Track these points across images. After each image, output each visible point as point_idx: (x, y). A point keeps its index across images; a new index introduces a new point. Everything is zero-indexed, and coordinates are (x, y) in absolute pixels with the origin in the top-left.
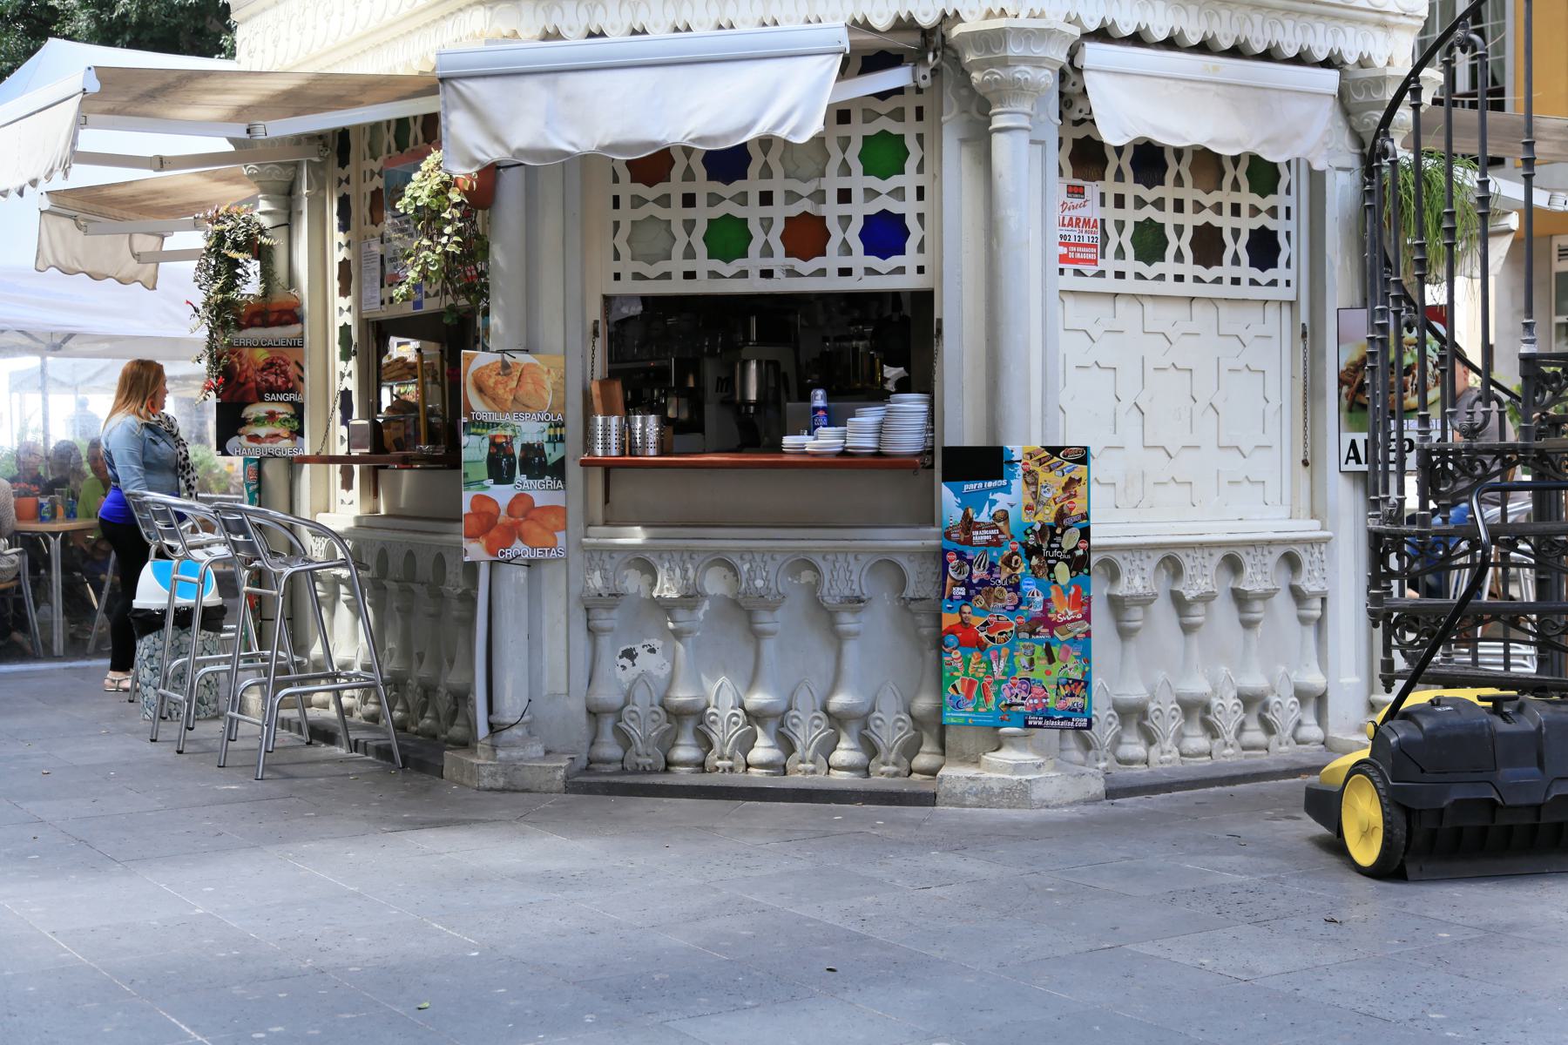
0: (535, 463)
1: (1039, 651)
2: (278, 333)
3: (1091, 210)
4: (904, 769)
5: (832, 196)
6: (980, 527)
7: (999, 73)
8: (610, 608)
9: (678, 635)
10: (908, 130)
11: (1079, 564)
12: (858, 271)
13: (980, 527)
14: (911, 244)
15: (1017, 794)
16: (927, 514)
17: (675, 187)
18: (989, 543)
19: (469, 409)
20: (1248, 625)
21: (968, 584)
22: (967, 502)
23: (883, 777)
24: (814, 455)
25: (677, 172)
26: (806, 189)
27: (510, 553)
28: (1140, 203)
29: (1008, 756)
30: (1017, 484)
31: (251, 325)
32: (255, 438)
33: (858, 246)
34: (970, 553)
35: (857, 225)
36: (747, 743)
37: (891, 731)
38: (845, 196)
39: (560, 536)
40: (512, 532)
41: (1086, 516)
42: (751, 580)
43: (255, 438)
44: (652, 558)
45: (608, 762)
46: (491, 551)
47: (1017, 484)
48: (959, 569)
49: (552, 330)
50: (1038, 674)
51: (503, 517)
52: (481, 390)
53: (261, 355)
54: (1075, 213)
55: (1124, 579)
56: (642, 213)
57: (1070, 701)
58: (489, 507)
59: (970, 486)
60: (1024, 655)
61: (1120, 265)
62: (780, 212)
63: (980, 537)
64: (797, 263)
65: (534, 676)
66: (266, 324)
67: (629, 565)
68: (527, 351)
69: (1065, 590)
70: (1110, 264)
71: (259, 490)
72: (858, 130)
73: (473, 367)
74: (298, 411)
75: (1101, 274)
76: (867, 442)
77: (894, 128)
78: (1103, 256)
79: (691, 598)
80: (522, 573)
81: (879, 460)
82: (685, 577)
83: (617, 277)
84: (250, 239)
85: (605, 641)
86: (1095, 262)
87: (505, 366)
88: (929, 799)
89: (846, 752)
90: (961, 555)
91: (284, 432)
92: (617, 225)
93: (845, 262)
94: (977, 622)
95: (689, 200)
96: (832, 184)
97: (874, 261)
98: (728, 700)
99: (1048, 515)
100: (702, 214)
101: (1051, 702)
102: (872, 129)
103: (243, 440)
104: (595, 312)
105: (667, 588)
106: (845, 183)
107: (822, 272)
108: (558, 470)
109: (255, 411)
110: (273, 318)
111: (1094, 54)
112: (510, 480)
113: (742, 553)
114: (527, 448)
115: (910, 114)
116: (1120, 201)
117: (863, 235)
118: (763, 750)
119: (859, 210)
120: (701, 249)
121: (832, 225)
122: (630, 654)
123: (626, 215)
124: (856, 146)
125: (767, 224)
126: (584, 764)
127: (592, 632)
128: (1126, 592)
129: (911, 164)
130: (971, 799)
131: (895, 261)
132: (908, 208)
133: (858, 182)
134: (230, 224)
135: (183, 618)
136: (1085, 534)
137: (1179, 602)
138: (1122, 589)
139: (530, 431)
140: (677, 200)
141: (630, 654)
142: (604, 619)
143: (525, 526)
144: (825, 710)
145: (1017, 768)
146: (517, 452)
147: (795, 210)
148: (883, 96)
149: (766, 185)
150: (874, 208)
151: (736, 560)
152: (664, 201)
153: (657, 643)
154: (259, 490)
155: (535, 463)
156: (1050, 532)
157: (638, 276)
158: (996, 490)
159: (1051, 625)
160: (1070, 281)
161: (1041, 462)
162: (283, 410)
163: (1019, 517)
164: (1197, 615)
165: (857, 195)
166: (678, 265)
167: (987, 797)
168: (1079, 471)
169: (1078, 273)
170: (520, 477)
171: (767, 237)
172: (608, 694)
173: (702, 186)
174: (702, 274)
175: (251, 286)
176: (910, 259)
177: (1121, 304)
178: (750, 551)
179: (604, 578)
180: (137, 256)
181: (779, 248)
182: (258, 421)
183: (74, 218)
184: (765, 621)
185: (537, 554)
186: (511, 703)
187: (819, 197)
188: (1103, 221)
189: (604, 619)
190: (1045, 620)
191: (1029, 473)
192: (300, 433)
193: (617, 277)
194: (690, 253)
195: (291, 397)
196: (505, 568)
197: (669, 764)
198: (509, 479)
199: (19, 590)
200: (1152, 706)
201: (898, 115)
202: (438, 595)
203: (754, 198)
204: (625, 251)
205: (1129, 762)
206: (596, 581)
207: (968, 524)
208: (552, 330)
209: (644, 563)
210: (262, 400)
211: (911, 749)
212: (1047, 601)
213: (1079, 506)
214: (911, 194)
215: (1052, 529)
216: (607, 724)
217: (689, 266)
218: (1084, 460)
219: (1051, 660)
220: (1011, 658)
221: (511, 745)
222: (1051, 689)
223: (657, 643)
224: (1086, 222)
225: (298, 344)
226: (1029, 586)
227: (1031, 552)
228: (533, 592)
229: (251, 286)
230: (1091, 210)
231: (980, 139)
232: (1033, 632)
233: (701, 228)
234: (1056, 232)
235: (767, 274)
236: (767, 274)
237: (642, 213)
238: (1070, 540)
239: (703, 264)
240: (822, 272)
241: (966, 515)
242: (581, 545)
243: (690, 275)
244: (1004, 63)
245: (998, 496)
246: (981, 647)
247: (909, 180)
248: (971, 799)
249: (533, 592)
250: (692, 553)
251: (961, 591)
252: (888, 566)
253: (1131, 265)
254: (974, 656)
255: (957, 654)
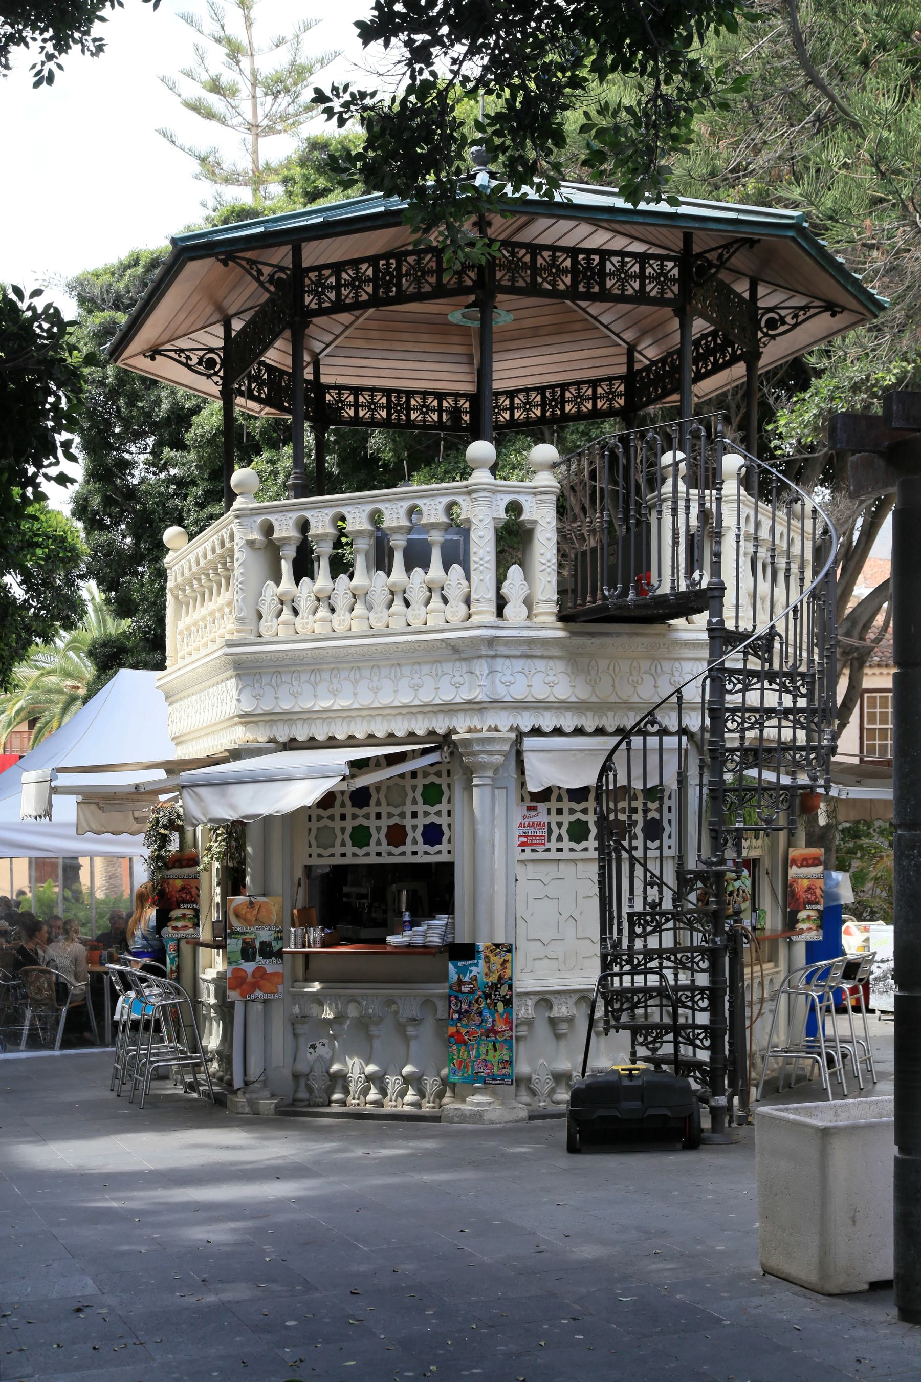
0: (267, 951)
1: (490, 1045)
2: (187, 871)
3: (542, 818)
4: (437, 1105)
5: (409, 815)
6: (465, 983)
7: (471, 759)
8: (303, 1023)
9: (334, 1037)
10: (443, 781)
11: (508, 1002)
12: (420, 853)
13: (465, 983)
14: (445, 839)
15: (477, 1117)
16: (444, 977)
17: (337, 811)
18: (469, 992)
19: (231, 926)
20: (558, 1037)
21: (459, 1012)
22: (462, 971)
23: (427, 1107)
24: (396, 947)
25: (337, 803)
26: (396, 811)
27: (253, 996)
28: (572, 811)
29: (478, 1098)
30: (481, 962)
31: (173, 867)
32: (175, 928)
33: (420, 840)
34: (461, 997)
35: (420, 829)
36: (365, 1091)
37: (431, 1084)
38: (414, 815)
39: (280, 987)
40: (255, 986)
41: (511, 979)
42: (367, 1009)
43: (175, 928)
44: (322, 998)
45: (302, 1101)
46: (243, 995)
47: (481, 962)
48: (456, 1005)
49: (278, 882)
50: (490, 1057)
51: (249, 979)
52: (237, 916)
53: (179, 883)
54: (531, 820)
55: (555, 1008)
56: (321, 824)
57: (504, 1071)
58: (243, 974)
59: (461, 963)
60: (484, 1048)
61: (560, 845)
62: (385, 823)
63: (465, 988)
64: (393, 849)
65: (266, 1058)
66: (182, 867)
67: (313, 1002)
68: (264, 895)
69: (501, 1015)
70: (553, 844)
71: (178, 956)
72: (420, 782)
73: (234, 905)
74: (197, 912)
75: (548, 850)
76: (419, 941)
77: (437, 780)
78: (549, 840)
79: (339, 1018)
80: (260, 1007)
81: (424, 950)
82: (337, 1008)
83: (310, 856)
84: (171, 821)
85: (302, 1040)
86: (544, 844)
87: (251, 903)
88: (436, 1119)
89: (411, 1096)
90: (457, 998)
91: (190, 925)
92: (310, 830)
93: (415, 848)
94: (463, 1031)
95: (343, 817)
96: (409, 809)
97: (428, 848)
98: (357, 1069)
99: (494, 978)
100: (349, 824)
101: (495, 1071)
102: (427, 781)
103: (170, 929)
104: (299, 873)
105: (328, 1014)
106: (414, 808)
107: (403, 854)
108: (280, 954)
109: (176, 913)
110: (184, 863)
111: (529, 743)
112: (253, 960)
113: (363, 996)
114: (262, 943)
115: (444, 774)
116: (560, 812)
117: (423, 835)
118: (373, 1095)
119: (421, 822)
120: (349, 842)
121: (409, 829)
122: (313, 1047)
123: (315, 825)
124: (420, 790)
125: (378, 829)
126: (290, 1100)
127: (295, 1035)
128: (557, 1015)
129: (445, 799)
130: (457, 1119)
131: (437, 848)
132: (443, 821)
133: (421, 808)
134: (162, 814)
135: (135, 1025)
136: (510, 987)
137: (553, 1022)
138: (555, 1013)
139: (265, 935)
140: (337, 817)
141: (313, 1047)
142: (301, 1029)
143: (262, 983)
144: (328, 1072)
145: (479, 1104)
146: (257, 945)
147: (391, 822)
148: (432, 765)
149: (378, 809)
150: (428, 821)
151: (359, 999)
152: (332, 818)
153: (326, 1041)
154: (178, 956)
155: (267, 951)
156: (495, 986)
157: (320, 856)
158: (472, 965)
159: (496, 1033)
160: (528, 855)
161: (492, 951)
162: (189, 913)
163: (483, 979)
164: (563, 1028)
165: (420, 814)
166: (338, 850)
167: (463, 1118)
168: (508, 956)
169: (533, 850)
170: (258, 958)
171: (379, 836)
172: (302, 1067)
173: (349, 810)
174: (349, 854)
175: (174, 846)
176: (444, 847)
177: (562, 866)
178: (366, 995)
179: (300, 1008)
180: (136, 819)
181: (384, 841)
182: (177, 919)
183: (97, 804)
184: (374, 1031)
185: (268, 996)
186: (255, 1070)
187: (402, 815)
188: (549, 823)
189: (301, 1029)
190: (492, 1031)
191: (487, 957)
192: (197, 925)
193: (310, 856)
194: (343, 844)
195: (194, 905)
196: (251, 1003)
197: (330, 1103)
198: (253, 959)
199: (85, 1005)
200: (534, 1077)
201: (438, 774)
202: (177, 1022)
203: (373, 816)
204: (314, 843)
205: (558, 1103)
206: (296, 1010)
207: (460, 982)
208: (278, 882)
209: (317, 999)
210: (179, 907)
211: (440, 1095)
212: (494, 1021)
213: (508, 973)
214: (445, 814)
215: (496, 985)
216: (302, 1082)
217: (343, 850)
218: (510, 951)
219: (496, 1050)
220: (478, 1049)
221: (253, 1092)
222: (495, 1065)
223: (326, 1041)
224: (538, 824)
225: (196, 877)
226: (486, 1013)
227: (487, 996)
228: (266, 1014)
229: (174, 846)
230: (542, 818)
231: (469, 787)
232: (488, 1037)
233: (349, 831)
234: (517, 831)
235: (379, 854)
236: (379, 854)
237: (321, 824)
238: (504, 990)
239: (350, 849)
240: (403, 854)
241: (459, 978)
242: (289, 992)
243: (343, 855)
244: (473, 754)
245: (473, 968)
246: (465, 1043)
247: (443, 807)
248: (457, 1119)
249: (266, 1014)
250: (340, 996)
251: (456, 1016)
252: (427, 1003)
253: (566, 844)
254: (462, 1048)
255: (455, 1047)
